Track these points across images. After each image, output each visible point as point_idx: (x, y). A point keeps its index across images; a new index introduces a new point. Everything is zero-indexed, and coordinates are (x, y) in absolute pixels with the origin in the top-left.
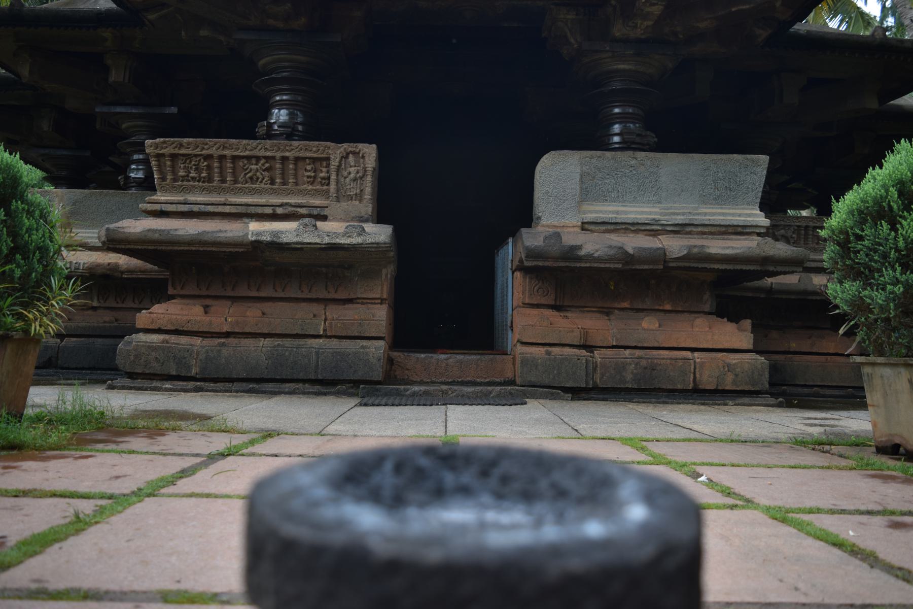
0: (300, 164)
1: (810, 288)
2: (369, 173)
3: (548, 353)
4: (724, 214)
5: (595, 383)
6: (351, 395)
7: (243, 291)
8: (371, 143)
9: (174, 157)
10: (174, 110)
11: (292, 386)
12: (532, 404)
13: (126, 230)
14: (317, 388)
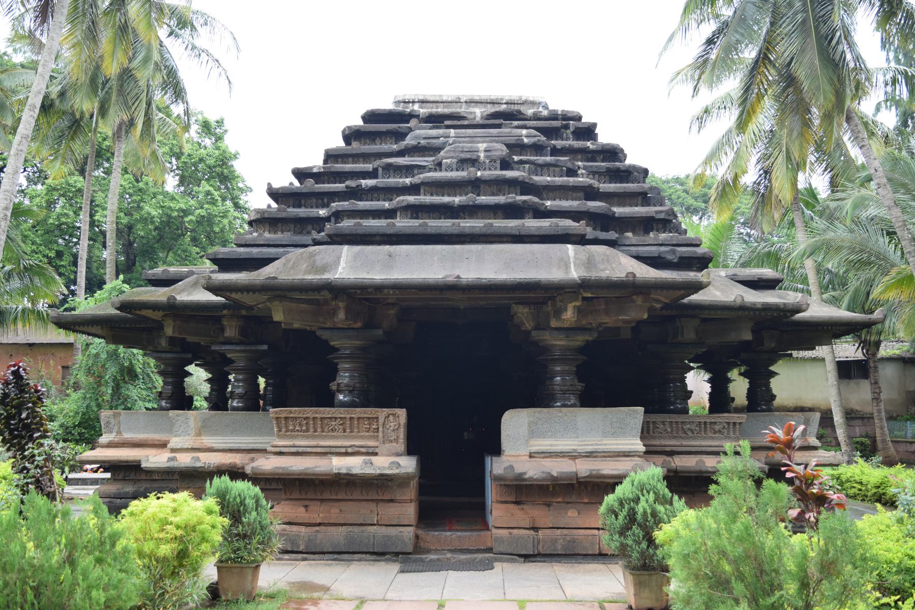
0: (361, 421)
1: (704, 469)
2: (402, 426)
3: (510, 533)
4: (617, 444)
6: (395, 561)
7: (326, 496)
8: (402, 408)
9: (286, 418)
10: (265, 347)
11: (359, 555)
14: (374, 557)
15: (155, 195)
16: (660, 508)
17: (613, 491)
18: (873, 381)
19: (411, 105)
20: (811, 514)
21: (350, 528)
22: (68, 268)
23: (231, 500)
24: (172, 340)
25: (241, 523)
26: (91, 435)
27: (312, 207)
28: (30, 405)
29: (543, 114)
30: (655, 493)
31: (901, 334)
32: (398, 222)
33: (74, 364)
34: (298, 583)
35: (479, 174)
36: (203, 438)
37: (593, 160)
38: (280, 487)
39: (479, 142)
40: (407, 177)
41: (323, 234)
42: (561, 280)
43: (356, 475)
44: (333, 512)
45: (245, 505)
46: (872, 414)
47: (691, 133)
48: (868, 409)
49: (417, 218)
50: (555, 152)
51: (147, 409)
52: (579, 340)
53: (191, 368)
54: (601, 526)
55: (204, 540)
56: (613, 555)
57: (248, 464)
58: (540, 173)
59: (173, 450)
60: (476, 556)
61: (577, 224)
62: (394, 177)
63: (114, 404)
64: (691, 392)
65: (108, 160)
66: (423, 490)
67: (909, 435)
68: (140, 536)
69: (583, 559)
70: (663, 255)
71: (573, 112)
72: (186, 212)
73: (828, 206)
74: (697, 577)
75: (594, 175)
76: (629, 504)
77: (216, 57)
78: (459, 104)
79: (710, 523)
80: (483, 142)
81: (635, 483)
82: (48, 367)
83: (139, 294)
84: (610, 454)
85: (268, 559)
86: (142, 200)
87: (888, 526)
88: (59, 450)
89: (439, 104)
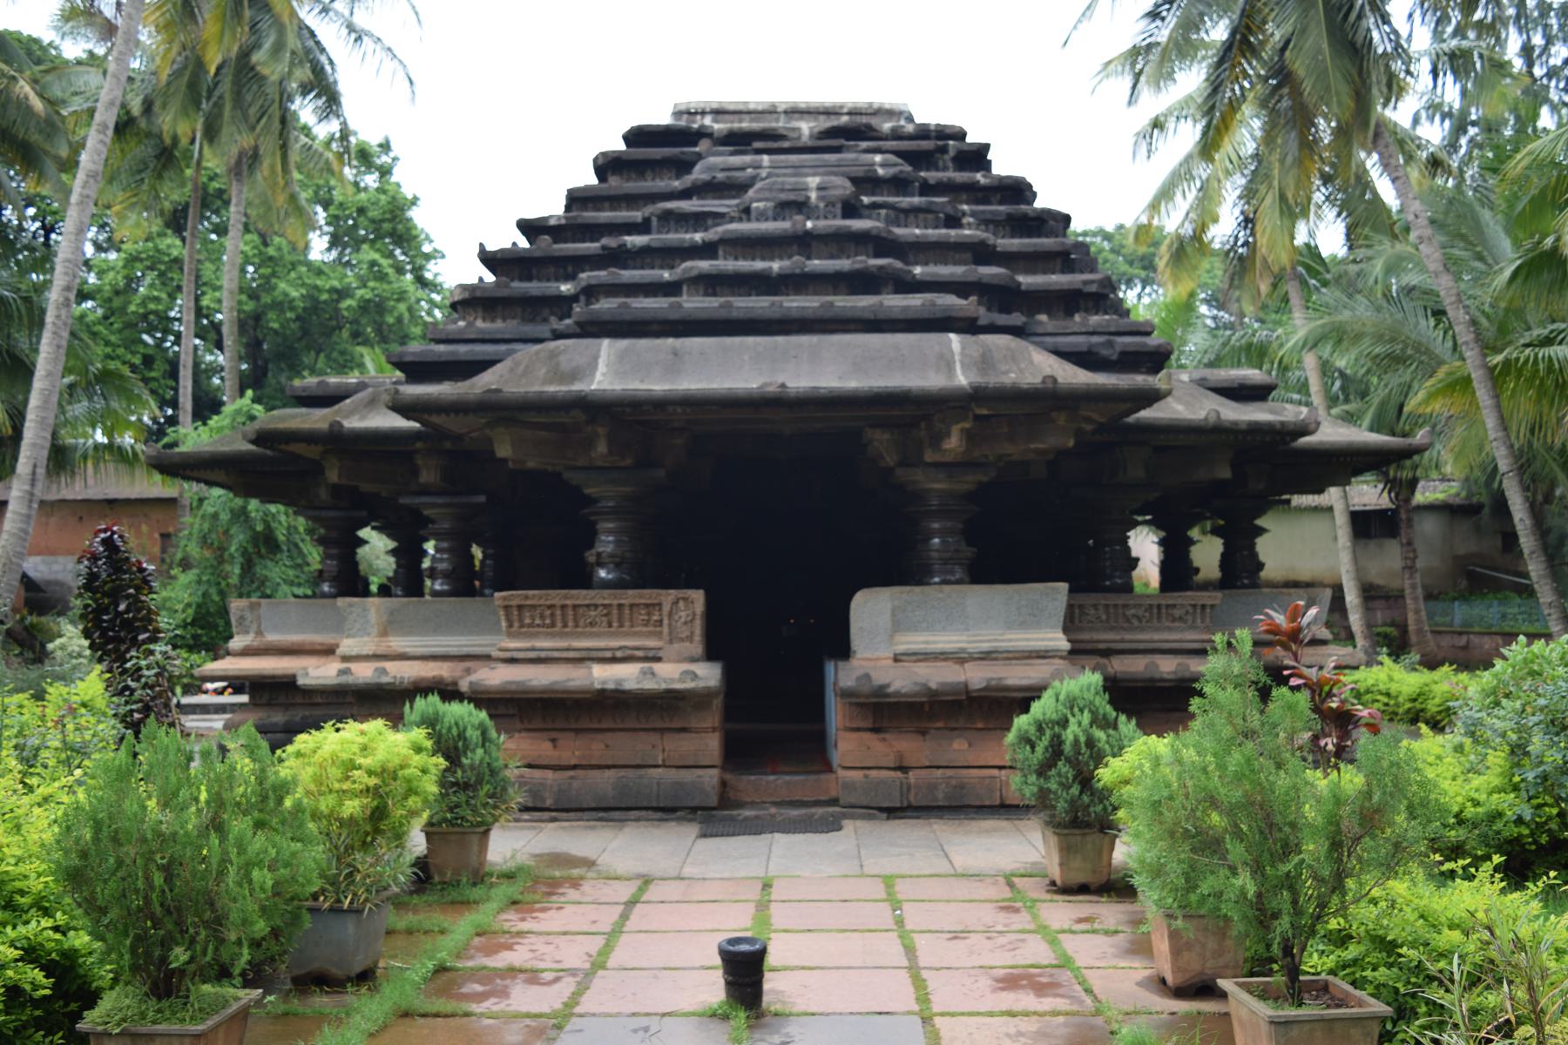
0: (635, 609)
1: (1157, 676)
2: (698, 617)
3: (866, 776)
4: (1028, 640)
5: (909, 802)
6: (690, 820)
7: (585, 723)
9: (520, 607)
10: (482, 499)
12: (848, 825)
14: (659, 815)
15: (294, 266)
16: (1100, 734)
17: (1026, 710)
18: (1404, 541)
19: (699, 117)
20: (1329, 740)
21: (622, 772)
22: (162, 381)
23: (444, 731)
24: (336, 490)
25: (460, 765)
26: (212, 638)
27: (548, 280)
28: (132, 591)
29: (905, 130)
30: (1090, 711)
31: (1448, 469)
32: (687, 301)
33: (180, 530)
34: (548, 854)
35: (809, 224)
36: (391, 638)
37: (985, 201)
38: (511, 712)
39: (808, 175)
40: (696, 231)
41: (568, 321)
42: (941, 389)
43: (629, 692)
44: (595, 747)
45: (465, 739)
46: (1403, 590)
47: (1138, 157)
48: (1395, 584)
49: (714, 295)
50: (927, 189)
51: (296, 596)
52: (968, 482)
53: (365, 533)
54: (1008, 764)
55: (411, 791)
56: (1028, 806)
57: (461, 678)
58: (903, 223)
59: (345, 659)
60: (813, 810)
61: (964, 302)
62: (676, 231)
63: (245, 590)
64: (1137, 560)
65: (217, 212)
66: (729, 714)
67: (1457, 621)
68: (312, 787)
69: (976, 813)
70: (1095, 350)
71: (953, 127)
72: (342, 293)
73: (1346, 273)
74: (1172, 834)
75: (986, 225)
76: (1052, 729)
77: (387, 43)
78: (775, 116)
79: (1190, 754)
80: (814, 175)
81: (1062, 697)
82: (139, 534)
83: (282, 419)
84: (1017, 655)
85: (502, 820)
86: (274, 274)
87: (1439, 757)
88: (180, 662)
89: (744, 116)
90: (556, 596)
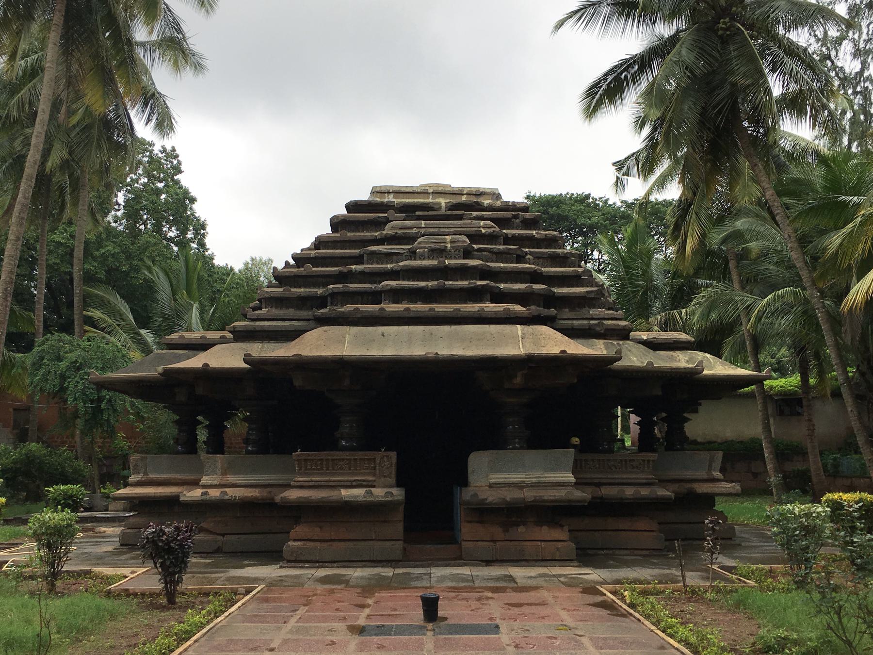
1: (624, 497)
4: (555, 477)
9: (305, 460)
13: (290, 498)
14: (373, 564)
50: (507, 240)
59: (204, 487)
70: (592, 327)
90: (323, 455)
